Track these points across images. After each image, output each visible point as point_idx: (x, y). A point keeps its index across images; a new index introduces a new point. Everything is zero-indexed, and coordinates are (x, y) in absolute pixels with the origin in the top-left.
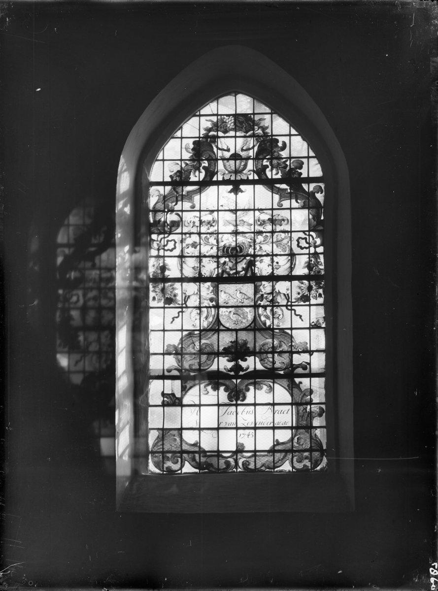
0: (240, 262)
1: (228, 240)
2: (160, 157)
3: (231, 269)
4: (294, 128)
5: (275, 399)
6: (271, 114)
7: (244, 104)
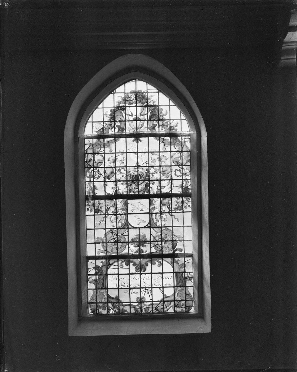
0: (140, 184)
1: (132, 171)
2: (90, 120)
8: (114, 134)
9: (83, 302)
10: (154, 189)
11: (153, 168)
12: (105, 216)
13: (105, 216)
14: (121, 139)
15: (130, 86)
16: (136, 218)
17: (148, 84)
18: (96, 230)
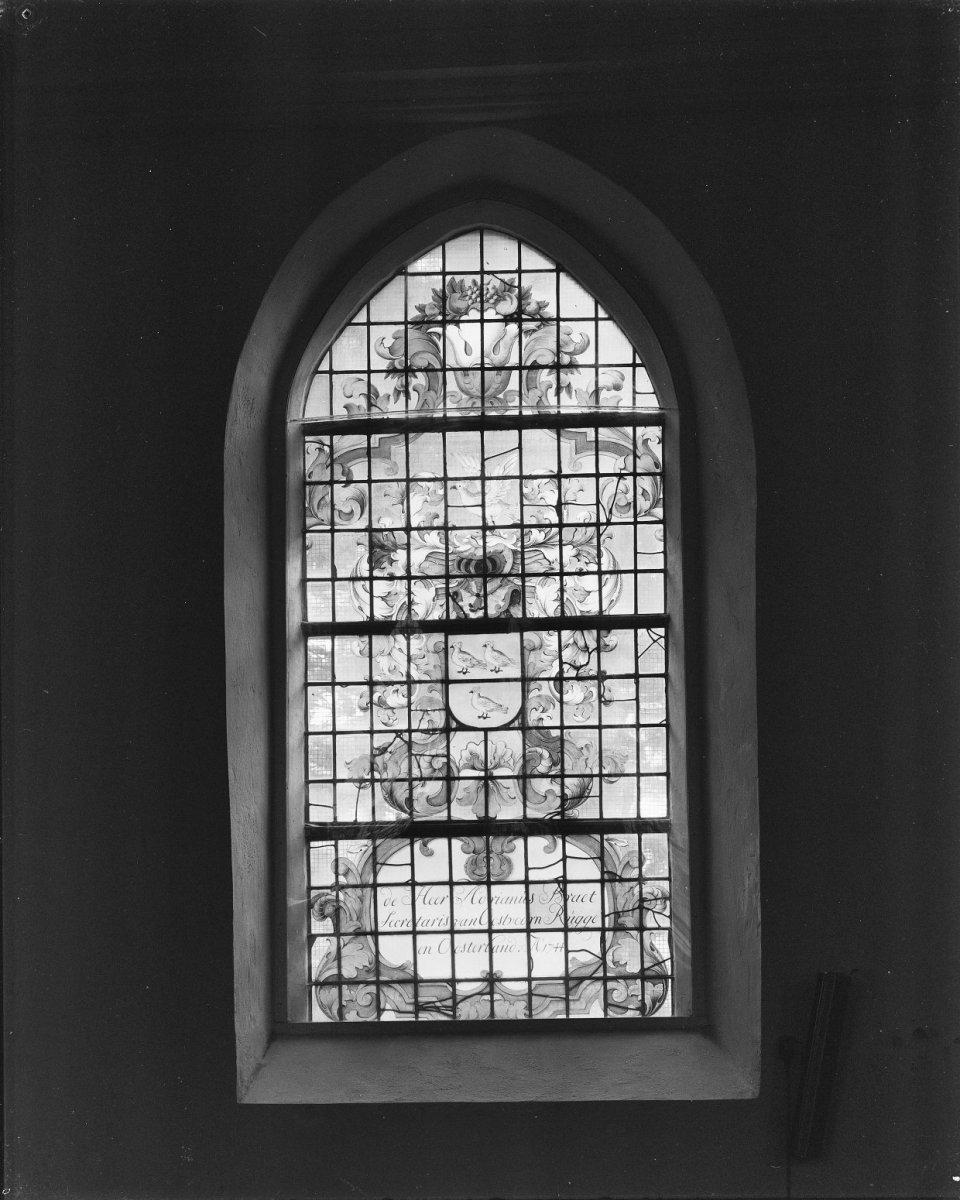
1: (466, 544)
3: (473, 608)
4: (531, 246)
5: (472, 524)
6: (634, 365)
7: (502, 253)
8: (403, 416)
9: (294, 981)
10: (543, 600)
11: (427, 586)
12: (377, 780)
13: (377, 780)
14: (427, 436)
15: (462, 254)
16: (475, 695)
17: (524, 248)
18: (342, 721)
